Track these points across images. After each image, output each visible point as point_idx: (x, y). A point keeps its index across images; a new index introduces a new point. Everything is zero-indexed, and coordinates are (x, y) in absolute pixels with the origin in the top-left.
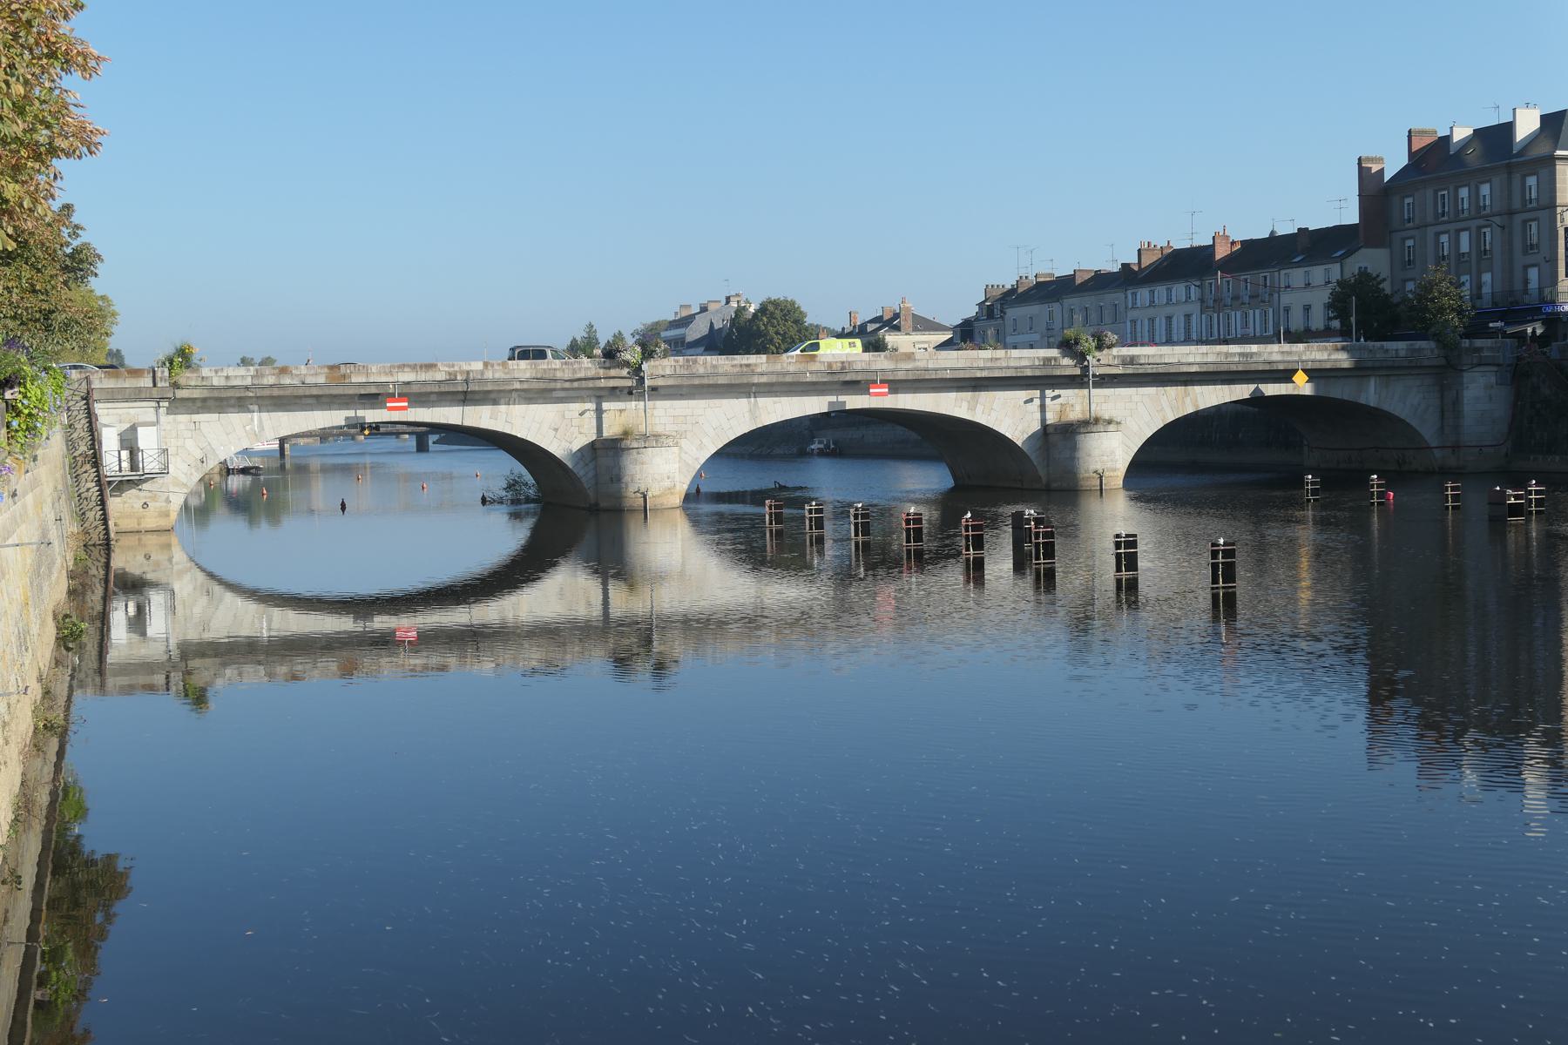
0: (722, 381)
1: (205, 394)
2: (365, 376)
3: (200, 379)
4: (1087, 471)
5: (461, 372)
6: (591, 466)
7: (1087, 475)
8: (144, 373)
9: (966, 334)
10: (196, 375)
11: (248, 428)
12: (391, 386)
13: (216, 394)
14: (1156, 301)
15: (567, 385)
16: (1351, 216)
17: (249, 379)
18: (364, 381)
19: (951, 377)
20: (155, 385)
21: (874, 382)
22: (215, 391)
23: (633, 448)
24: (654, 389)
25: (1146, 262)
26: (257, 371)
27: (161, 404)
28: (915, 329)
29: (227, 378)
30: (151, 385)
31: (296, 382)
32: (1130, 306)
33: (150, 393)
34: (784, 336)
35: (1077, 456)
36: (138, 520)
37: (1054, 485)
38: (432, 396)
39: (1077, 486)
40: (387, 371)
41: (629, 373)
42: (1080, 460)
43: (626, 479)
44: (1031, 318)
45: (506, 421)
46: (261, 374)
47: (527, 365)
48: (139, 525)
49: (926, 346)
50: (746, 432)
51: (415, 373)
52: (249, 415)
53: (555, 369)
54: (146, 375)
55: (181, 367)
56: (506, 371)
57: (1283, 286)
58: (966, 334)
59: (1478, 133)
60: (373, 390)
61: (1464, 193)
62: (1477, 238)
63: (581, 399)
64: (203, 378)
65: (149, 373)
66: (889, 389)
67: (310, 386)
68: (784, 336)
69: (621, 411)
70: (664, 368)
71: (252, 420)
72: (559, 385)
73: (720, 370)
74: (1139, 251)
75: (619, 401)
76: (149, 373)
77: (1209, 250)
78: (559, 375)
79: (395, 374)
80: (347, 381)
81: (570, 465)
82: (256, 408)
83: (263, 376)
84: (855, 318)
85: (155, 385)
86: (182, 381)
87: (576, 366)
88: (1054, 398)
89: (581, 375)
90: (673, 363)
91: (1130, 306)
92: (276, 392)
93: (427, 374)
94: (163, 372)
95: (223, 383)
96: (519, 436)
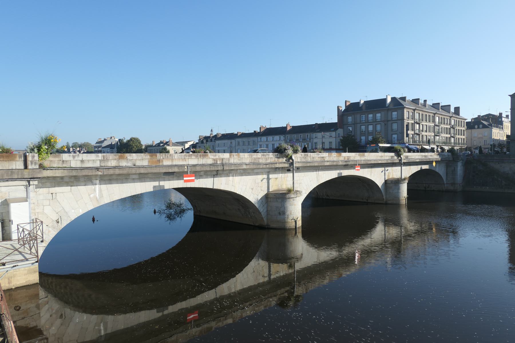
0: (316, 164)
1: (65, 173)
2: (171, 161)
3: (61, 162)
4: (402, 197)
5: (220, 159)
6: (265, 206)
7: (402, 198)
8: (15, 157)
9: (195, 148)
10: (57, 159)
11: (92, 196)
12: (186, 167)
13: (74, 173)
14: (269, 140)
15: (264, 166)
16: (335, 120)
17: (98, 162)
18: (170, 164)
19: (342, 164)
20: (26, 167)
21: (356, 165)
22: (74, 171)
23: (292, 198)
24: (298, 168)
25: (262, 130)
26: (104, 157)
27: (31, 183)
28: (173, 145)
29: (82, 161)
30: (22, 167)
31: (130, 164)
32: (259, 141)
33: (22, 174)
34: (137, 146)
35: (400, 192)
36: (9, 279)
37: (390, 202)
38: (202, 172)
39: (399, 202)
40: (183, 158)
41: (286, 160)
42: (401, 193)
43: (288, 213)
44: (224, 144)
45: (232, 186)
46: (107, 159)
47: (248, 155)
48: (9, 283)
49: (175, 149)
50: (315, 186)
51: (197, 159)
52: (93, 187)
53: (259, 158)
54: (18, 159)
55: (47, 153)
56: (239, 159)
57: (314, 137)
58: (195, 148)
59: (365, 102)
60: (176, 170)
61: (371, 116)
62: (375, 128)
63: (262, 173)
64: (63, 161)
65: (20, 157)
66: (360, 167)
67: (139, 167)
68: (137, 146)
69: (276, 178)
70: (374, 162)
71: (95, 190)
72: (261, 167)
73: (315, 160)
74: (260, 128)
75: (276, 174)
76: (20, 157)
77: (286, 128)
78: (261, 161)
79: (187, 160)
80: (161, 164)
81: (256, 205)
82: (98, 181)
83: (107, 160)
84: (154, 142)
85: (26, 167)
86: (46, 164)
87: (267, 157)
88: (388, 170)
89: (269, 161)
90: (301, 156)
91: (259, 141)
92: (117, 171)
93: (203, 160)
94: (33, 157)
95: (79, 165)
96: (237, 193)
